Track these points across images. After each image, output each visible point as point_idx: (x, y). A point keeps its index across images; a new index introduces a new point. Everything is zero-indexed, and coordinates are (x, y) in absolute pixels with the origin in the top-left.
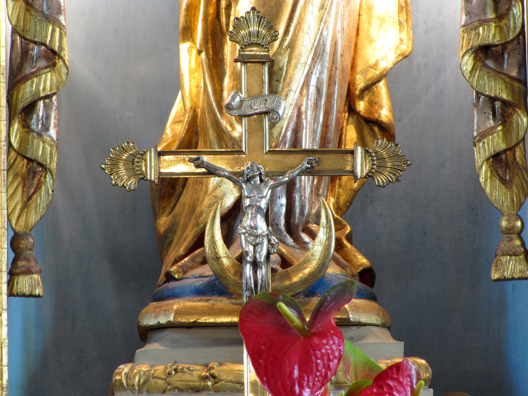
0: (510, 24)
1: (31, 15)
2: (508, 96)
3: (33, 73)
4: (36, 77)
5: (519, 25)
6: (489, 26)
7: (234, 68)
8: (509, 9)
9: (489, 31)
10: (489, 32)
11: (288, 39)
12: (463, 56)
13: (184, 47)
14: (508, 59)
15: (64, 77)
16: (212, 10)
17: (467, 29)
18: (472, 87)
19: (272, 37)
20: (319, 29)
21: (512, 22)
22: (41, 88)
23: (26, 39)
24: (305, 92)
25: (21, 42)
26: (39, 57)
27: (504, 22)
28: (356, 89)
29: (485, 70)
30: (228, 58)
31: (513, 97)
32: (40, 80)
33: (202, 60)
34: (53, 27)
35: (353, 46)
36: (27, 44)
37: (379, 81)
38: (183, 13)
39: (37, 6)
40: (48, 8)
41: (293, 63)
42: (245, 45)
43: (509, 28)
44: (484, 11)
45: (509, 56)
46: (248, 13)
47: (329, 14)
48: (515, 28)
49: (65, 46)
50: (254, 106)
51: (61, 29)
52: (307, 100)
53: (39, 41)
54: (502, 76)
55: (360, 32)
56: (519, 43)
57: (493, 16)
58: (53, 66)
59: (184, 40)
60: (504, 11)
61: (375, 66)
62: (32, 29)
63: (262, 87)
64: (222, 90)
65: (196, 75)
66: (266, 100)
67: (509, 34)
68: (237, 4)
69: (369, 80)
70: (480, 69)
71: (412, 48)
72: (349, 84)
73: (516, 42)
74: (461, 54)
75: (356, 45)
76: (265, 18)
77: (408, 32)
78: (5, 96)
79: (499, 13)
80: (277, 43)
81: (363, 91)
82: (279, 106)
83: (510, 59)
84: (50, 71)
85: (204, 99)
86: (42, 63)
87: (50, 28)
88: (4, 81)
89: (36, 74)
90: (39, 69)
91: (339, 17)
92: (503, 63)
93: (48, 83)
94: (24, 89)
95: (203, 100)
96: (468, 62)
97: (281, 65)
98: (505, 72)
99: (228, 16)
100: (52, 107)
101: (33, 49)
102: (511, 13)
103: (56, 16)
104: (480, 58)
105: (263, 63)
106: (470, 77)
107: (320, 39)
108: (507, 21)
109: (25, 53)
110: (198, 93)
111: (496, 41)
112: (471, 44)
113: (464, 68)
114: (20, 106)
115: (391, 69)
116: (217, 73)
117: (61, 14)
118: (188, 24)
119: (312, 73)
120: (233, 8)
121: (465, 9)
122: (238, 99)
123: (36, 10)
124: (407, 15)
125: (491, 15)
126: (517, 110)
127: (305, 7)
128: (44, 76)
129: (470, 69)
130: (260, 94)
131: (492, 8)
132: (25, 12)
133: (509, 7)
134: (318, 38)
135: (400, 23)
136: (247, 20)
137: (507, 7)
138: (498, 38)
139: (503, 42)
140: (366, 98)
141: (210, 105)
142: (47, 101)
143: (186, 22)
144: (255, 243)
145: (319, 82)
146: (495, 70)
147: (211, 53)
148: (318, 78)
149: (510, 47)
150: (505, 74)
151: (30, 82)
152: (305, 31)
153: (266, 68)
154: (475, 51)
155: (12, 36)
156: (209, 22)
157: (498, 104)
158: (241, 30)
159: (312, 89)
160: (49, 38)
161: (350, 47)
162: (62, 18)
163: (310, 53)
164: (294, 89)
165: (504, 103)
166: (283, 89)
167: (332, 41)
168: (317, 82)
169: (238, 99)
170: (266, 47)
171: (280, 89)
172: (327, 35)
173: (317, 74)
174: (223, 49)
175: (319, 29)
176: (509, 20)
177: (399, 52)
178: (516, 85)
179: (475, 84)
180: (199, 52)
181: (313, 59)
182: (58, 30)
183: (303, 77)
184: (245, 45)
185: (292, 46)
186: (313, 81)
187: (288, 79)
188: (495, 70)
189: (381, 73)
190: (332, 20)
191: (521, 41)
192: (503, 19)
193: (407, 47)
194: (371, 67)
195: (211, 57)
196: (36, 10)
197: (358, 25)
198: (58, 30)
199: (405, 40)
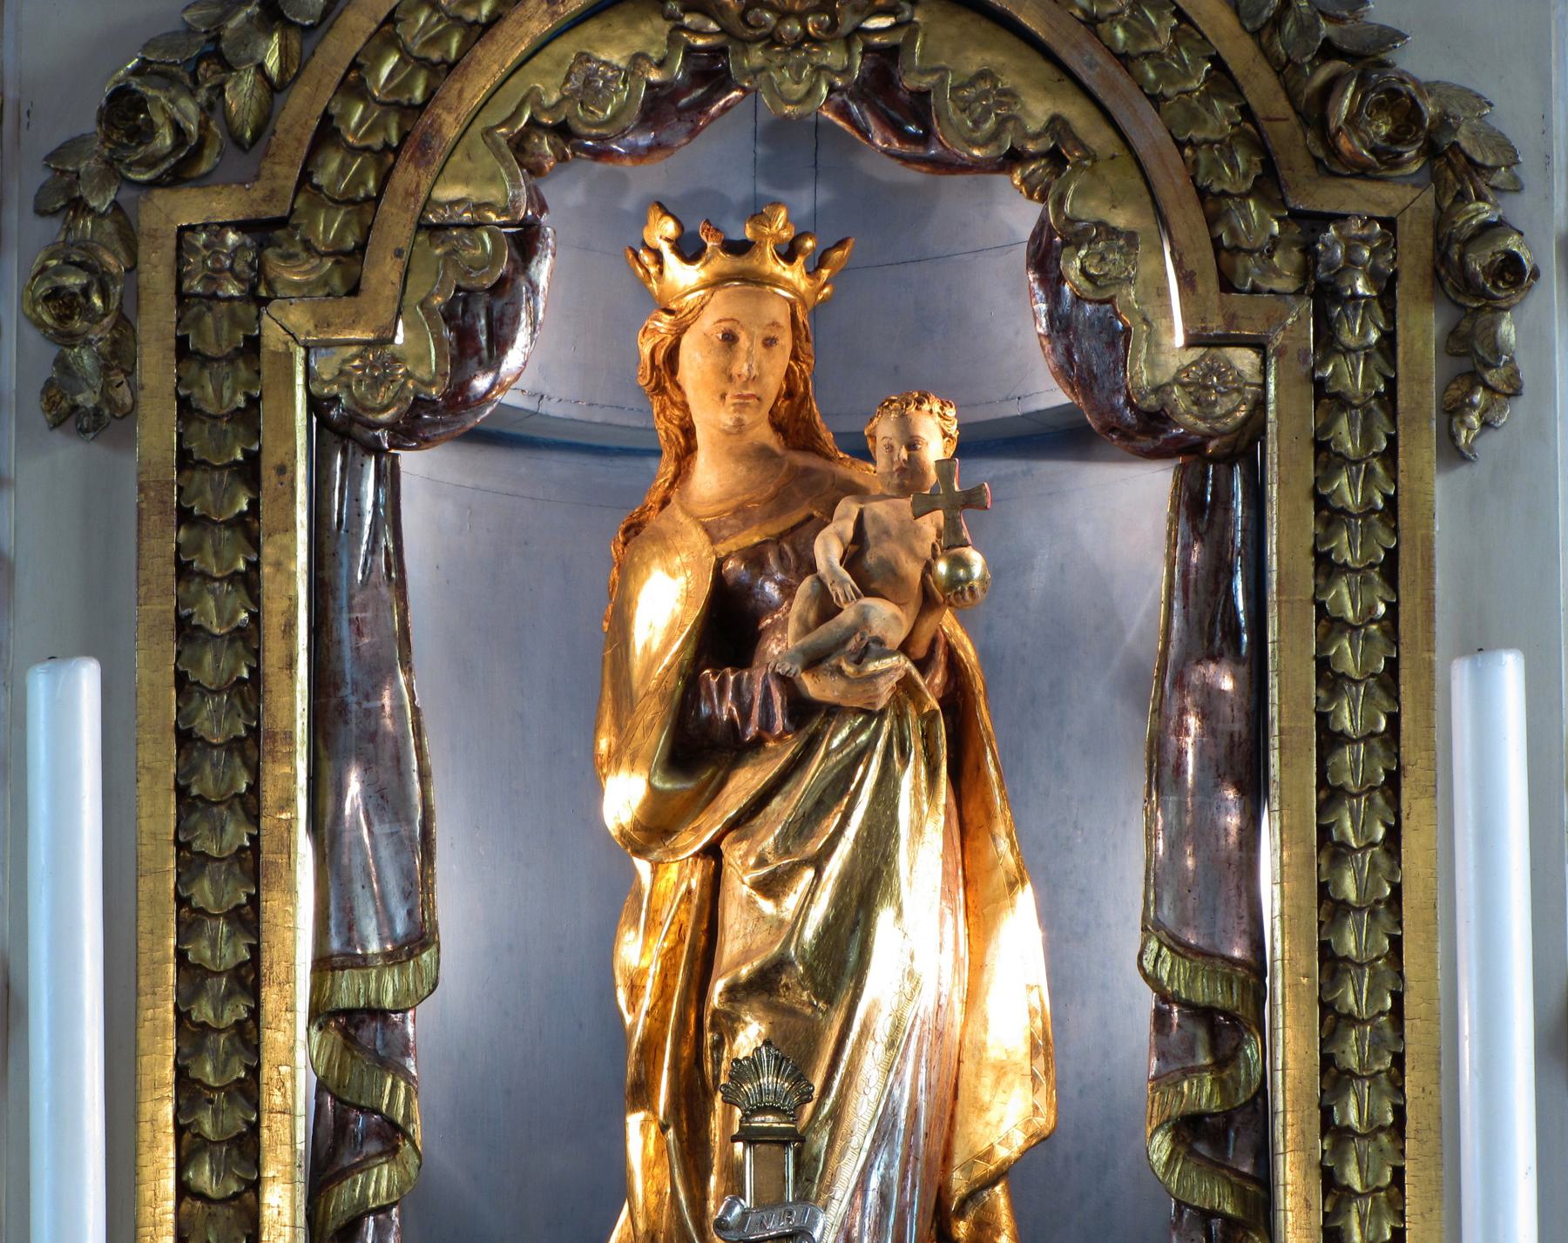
0: (1240, 1075)
1: (353, 1057)
2: (1235, 1208)
3: (356, 1165)
4: (361, 1172)
5: (1256, 1075)
6: (1200, 1081)
7: (728, 1157)
8: (1238, 1048)
9: (1201, 1087)
10: (1201, 1091)
11: (829, 1102)
12: (1152, 1136)
13: (634, 1120)
14: (1235, 1140)
15: (413, 1173)
16: (686, 1051)
17: (1159, 1085)
18: (1169, 1192)
19: (802, 1095)
20: (885, 1085)
21: (1243, 1071)
22: (371, 1192)
23: (343, 1102)
24: (858, 1202)
25: (334, 1107)
26: (368, 1134)
27: (1228, 1072)
28: (952, 1199)
29: (1193, 1161)
30: (717, 1139)
31: (1244, 1211)
32: (368, 1178)
33: (668, 1142)
34: (393, 1079)
35: (947, 1118)
36: (345, 1111)
37: (994, 1183)
38: (633, 1056)
39: (364, 1041)
40: (386, 1045)
41: (837, 1149)
42: (752, 1111)
43: (1237, 1082)
44: (1191, 1051)
45: (1236, 1134)
46: (757, 1049)
47: (904, 1057)
48: (1249, 1082)
49: (416, 1115)
50: (768, 1222)
51: (408, 1083)
52: (863, 1216)
53: (369, 1105)
54: (1225, 1172)
55: (961, 1093)
56: (1256, 1110)
57: (1208, 1061)
58: (391, 1151)
59: (635, 1108)
60: (1228, 1052)
61: (988, 1155)
62: (356, 1083)
63: (783, 1190)
64: (705, 1199)
65: (657, 1171)
66: (791, 1213)
67: (1237, 1094)
68: (734, 1039)
69: (977, 1181)
70: (1184, 1159)
71: (1056, 1122)
72: (940, 1188)
73: (1250, 1109)
74: (1149, 1131)
75: (952, 1117)
76: (788, 1060)
77: (1049, 1093)
78: (303, 1207)
79: (1220, 1055)
80: (809, 1107)
81: (964, 1202)
82: (813, 1223)
83: (1239, 1140)
84: (387, 1162)
85: (670, 1217)
86: (372, 1147)
87: (389, 1081)
88: (303, 1179)
89: (363, 1166)
90: (368, 1158)
91: (923, 1063)
92: (1227, 1148)
93: (384, 1183)
94: (339, 1194)
95: (669, 1217)
96: (1160, 1147)
97: (815, 1150)
98: (1229, 1164)
99: (717, 1063)
100: (391, 1229)
101: (356, 1121)
102: (1241, 1055)
103: (400, 1060)
104: (1184, 1139)
105: (785, 1144)
106: (1164, 1174)
107: (886, 1104)
108: (1233, 1071)
109: (341, 1126)
110: (660, 1204)
111: (1213, 1106)
112: (1167, 1112)
113: (1155, 1157)
114: (331, 1226)
115: (1017, 1160)
116: (696, 1167)
117: (409, 1055)
118: (643, 1077)
119: (872, 1166)
120: (727, 1047)
121: (1157, 1047)
122: (737, 1210)
123: (363, 1049)
124: (1047, 1062)
125: (1204, 1059)
126: (1252, 1234)
127: (860, 1043)
128: (376, 1171)
129: (1164, 1158)
130: (781, 1201)
131: (1207, 1047)
132: (342, 1052)
133: (1238, 1044)
134: (883, 1102)
135: (1034, 1077)
136: (755, 1064)
137: (1234, 1044)
138: (1217, 1101)
139: (1227, 1108)
140: (971, 1216)
141: (682, 1225)
142: (381, 1216)
143: (639, 1074)
144: (1383, 793)
145: (885, 1182)
146: (1210, 1161)
147: (685, 1129)
148: (883, 1177)
149: (1239, 1118)
150: (1230, 1169)
151: (349, 1181)
152: (860, 1089)
153: (791, 1153)
154: (1174, 1125)
155: (317, 1097)
156: (682, 1073)
157: (1216, 1224)
158: (745, 1082)
159: (872, 1197)
160: (386, 1100)
161: (942, 1121)
162: (410, 1064)
163: (869, 1129)
164: (838, 1195)
165: (1227, 1219)
166: (818, 1196)
167: (909, 1108)
168: (881, 1184)
169: (737, 1210)
170: (793, 1114)
171: (813, 1196)
172: (901, 1095)
173: (881, 1169)
174: (708, 1123)
175: (885, 1085)
176: (1238, 1068)
177: (1031, 1130)
178: (1251, 1188)
179: (1174, 1186)
180: (663, 1129)
181: (874, 1141)
182: (402, 1084)
183: (856, 1174)
184: (752, 1111)
185: (836, 1116)
186: (874, 1182)
187: (828, 1178)
188: (1210, 1161)
189: (998, 1168)
190: (909, 1069)
191: (1260, 1108)
192: (1226, 1066)
193: (1044, 1121)
194: (980, 1158)
195: (684, 1137)
196: (363, 1049)
197: (957, 1079)
198: (402, 1084)
199: (1043, 1109)
